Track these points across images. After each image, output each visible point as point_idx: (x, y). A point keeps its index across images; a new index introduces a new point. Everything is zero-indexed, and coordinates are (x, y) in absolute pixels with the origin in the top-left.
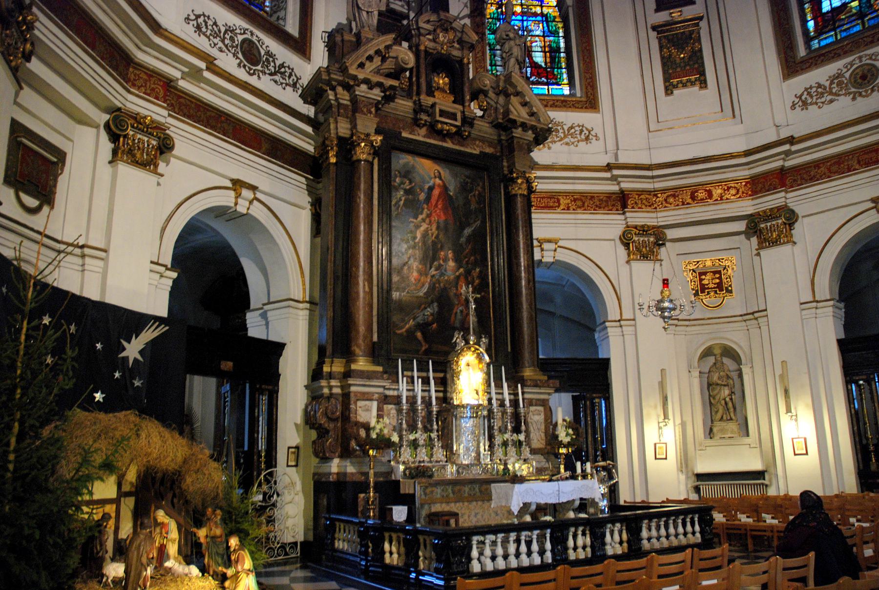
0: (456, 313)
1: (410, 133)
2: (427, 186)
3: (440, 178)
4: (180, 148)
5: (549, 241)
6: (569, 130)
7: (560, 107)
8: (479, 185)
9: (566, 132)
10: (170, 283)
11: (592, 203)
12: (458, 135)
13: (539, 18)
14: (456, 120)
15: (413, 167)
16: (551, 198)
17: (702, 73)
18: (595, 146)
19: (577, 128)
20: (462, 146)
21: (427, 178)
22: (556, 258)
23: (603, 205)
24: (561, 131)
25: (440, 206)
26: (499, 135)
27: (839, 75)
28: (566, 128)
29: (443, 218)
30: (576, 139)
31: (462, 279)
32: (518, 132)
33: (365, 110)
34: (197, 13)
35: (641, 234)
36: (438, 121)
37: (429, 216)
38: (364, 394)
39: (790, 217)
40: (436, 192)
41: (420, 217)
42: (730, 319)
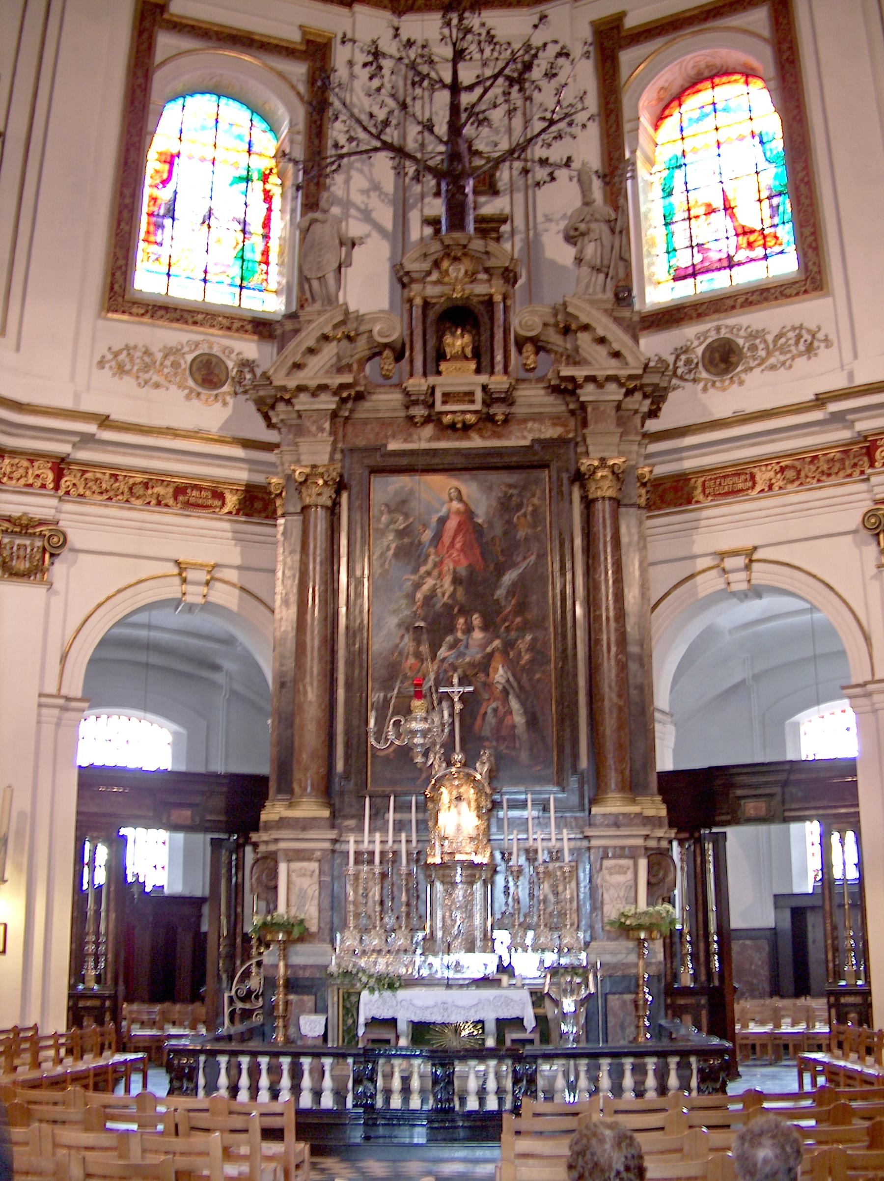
0: (486, 713)
1: (405, 441)
2: (435, 518)
3: (460, 499)
5: (735, 553)
6: (775, 341)
7: (758, 302)
8: (533, 495)
9: (771, 346)
11: (813, 468)
14: (472, 402)
15: (411, 492)
16: (739, 475)
18: (825, 356)
20: (499, 436)
22: (753, 582)
23: (835, 469)
24: (761, 346)
25: (458, 546)
28: (770, 338)
29: (464, 563)
30: (789, 356)
31: (497, 656)
32: (588, 393)
33: (314, 429)
34: (116, 348)
37: (438, 565)
38: (297, 851)
41: (423, 570)
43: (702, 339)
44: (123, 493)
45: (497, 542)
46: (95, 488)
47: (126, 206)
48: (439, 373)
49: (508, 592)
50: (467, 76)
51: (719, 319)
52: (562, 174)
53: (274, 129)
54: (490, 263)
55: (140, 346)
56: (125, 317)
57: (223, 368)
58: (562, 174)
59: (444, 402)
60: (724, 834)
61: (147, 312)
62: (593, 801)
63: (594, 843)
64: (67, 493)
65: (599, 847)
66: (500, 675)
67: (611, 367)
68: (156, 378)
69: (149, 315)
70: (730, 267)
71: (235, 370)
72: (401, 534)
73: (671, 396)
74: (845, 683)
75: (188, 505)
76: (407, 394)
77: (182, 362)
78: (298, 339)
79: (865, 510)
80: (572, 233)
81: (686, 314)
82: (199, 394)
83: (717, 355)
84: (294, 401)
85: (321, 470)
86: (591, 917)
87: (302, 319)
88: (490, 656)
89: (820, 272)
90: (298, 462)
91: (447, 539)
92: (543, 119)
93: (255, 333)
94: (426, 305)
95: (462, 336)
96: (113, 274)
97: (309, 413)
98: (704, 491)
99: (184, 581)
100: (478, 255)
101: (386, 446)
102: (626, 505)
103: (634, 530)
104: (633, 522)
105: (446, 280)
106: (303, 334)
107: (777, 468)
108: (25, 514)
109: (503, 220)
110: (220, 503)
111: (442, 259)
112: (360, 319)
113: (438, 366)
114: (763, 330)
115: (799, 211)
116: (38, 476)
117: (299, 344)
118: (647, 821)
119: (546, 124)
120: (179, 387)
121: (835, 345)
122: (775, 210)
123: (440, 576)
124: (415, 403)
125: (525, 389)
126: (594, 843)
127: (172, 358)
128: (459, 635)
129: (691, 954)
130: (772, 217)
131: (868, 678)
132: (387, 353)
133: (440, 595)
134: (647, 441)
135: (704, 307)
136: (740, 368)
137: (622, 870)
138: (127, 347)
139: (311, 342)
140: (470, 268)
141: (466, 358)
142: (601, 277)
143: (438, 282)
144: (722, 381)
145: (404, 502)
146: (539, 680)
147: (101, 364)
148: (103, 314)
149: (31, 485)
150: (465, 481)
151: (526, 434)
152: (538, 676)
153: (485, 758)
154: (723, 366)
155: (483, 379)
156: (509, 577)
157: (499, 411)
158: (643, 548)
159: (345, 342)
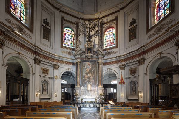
4: (146, 58)
10: (7, 68)
12: (92, 58)
17: (136, 36)
18: (117, 53)
27: (155, 30)
39: (58, 67)
42: (135, 77)
50: (90, 27)
66: (92, 77)
67: (100, 54)
156: (93, 70)
157: (92, 57)
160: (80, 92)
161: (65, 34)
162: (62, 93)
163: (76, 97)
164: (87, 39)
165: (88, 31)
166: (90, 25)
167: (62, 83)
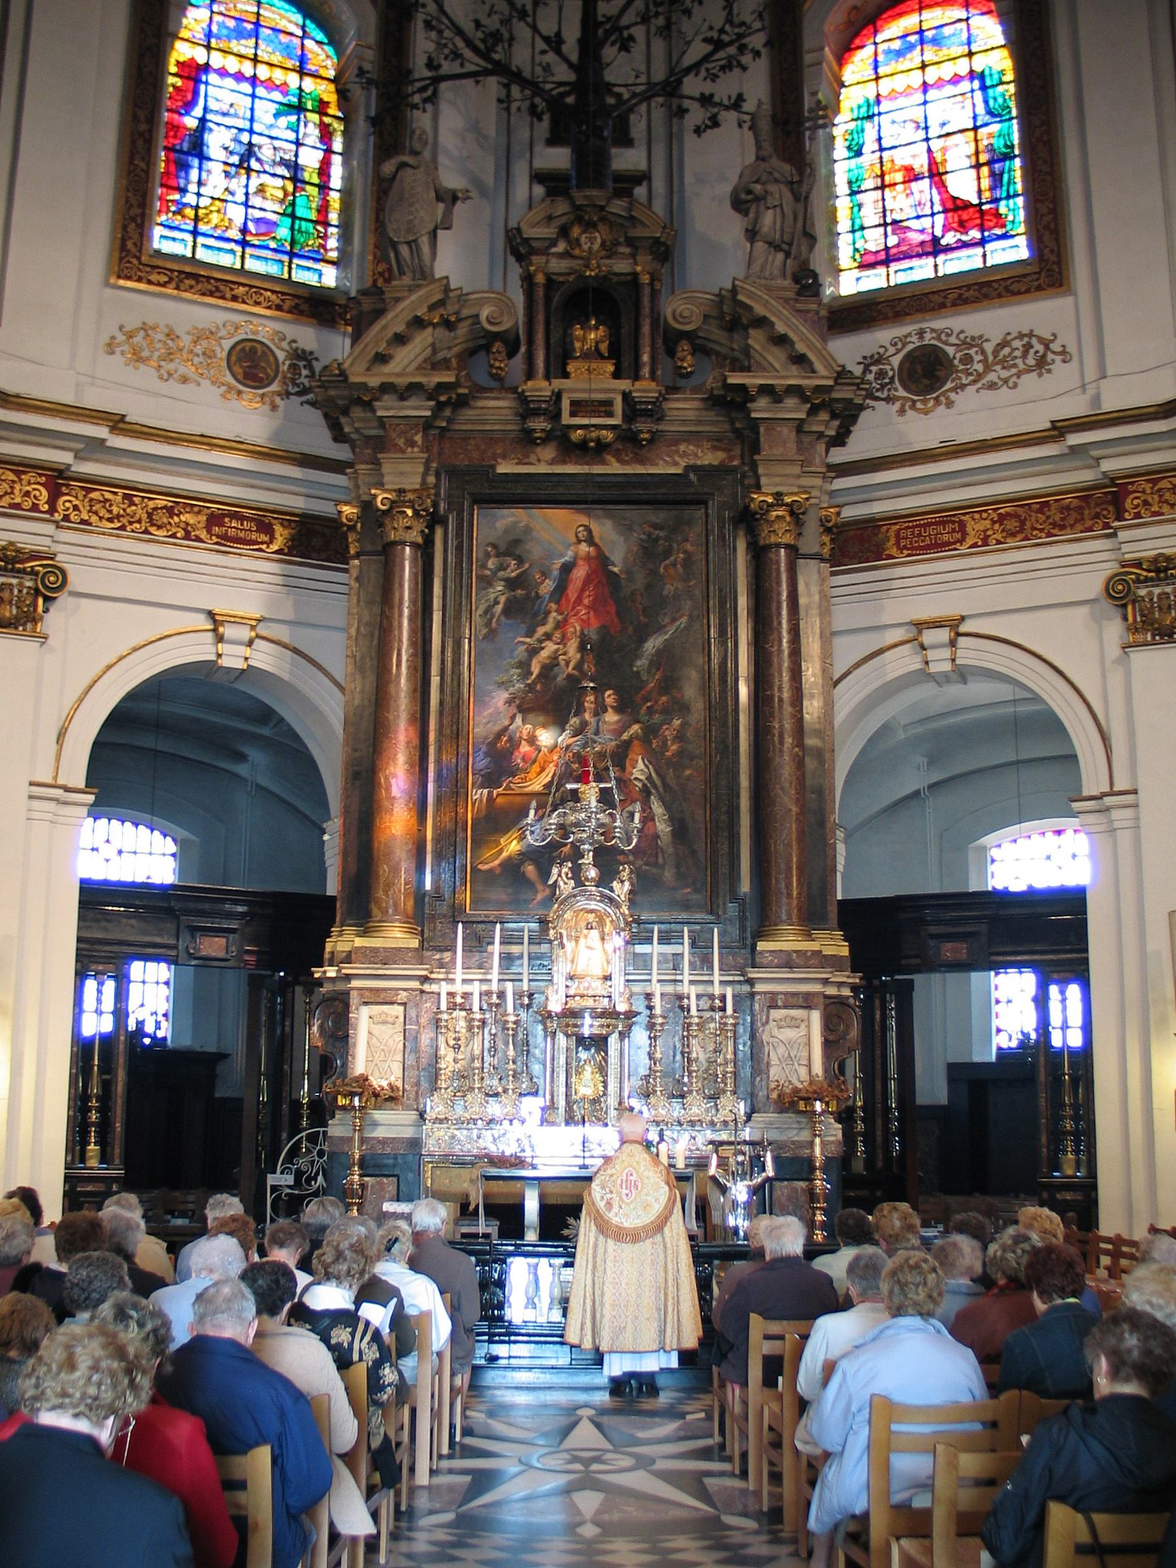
3: (590, 540)
5: (936, 624)
6: (996, 352)
7: (976, 300)
9: (991, 358)
11: (1042, 517)
13: (965, 86)
14: (610, 414)
15: (528, 530)
16: (943, 523)
18: (1062, 374)
19: (1017, 344)
20: (642, 462)
21: (560, 547)
25: (586, 601)
26: (732, 422)
28: (989, 347)
29: (595, 624)
30: (1014, 371)
31: (636, 746)
33: (401, 442)
35: (1152, 579)
36: (570, 427)
40: (580, 573)
41: (541, 630)
43: (899, 346)
44: (139, 521)
45: (639, 598)
46: (102, 513)
47: (141, 134)
48: (566, 375)
49: (651, 662)
51: (924, 320)
52: (729, 118)
53: (334, 40)
54: (639, 232)
55: (162, 325)
56: (142, 286)
57: (271, 359)
58: (729, 118)
59: (573, 414)
60: (912, 980)
61: (171, 280)
62: (761, 933)
63: (759, 988)
64: (66, 518)
65: (765, 993)
68: (182, 370)
69: (173, 285)
70: (935, 254)
71: (287, 363)
72: (511, 584)
73: (864, 416)
74: (1074, 795)
75: (225, 538)
76: (523, 399)
77: (218, 350)
78: (382, 322)
79: (1108, 573)
80: (743, 196)
81: (879, 312)
82: (239, 393)
83: (919, 368)
84: (377, 404)
85: (410, 496)
86: (753, 1083)
87: (387, 295)
88: (626, 745)
89: (1059, 263)
90: (380, 485)
91: (572, 593)
92: (707, 40)
93: (312, 316)
94: (550, 283)
95: (596, 328)
96: (125, 227)
97: (396, 421)
98: (897, 544)
99: (220, 639)
100: (619, 220)
101: (493, 467)
102: (806, 557)
103: (815, 589)
104: (815, 577)
105: (577, 252)
106: (390, 315)
107: (995, 516)
108: (11, 543)
109: (642, 178)
110: (266, 539)
111: (572, 223)
112: (463, 298)
113: (564, 365)
114: (981, 337)
115: (1034, 180)
116: (27, 494)
117: (384, 328)
118: (822, 960)
119: (710, 48)
120: (214, 383)
121: (1075, 358)
122: (996, 178)
123: (563, 640)
124: (536, 413)
125: (678, 400)
126: (759, 988)
127: (204, 343)
128: (587, 716)
129: (863, 1135)
130: (992, 189)
131: (1106, 788)
132: (497, 346)
133: (563, 663)
134: (833, 474)
135: (904, 303)
136: (949, 385)
137: (794, 1024)
138: (144, 328)
139: (400, 328)
140: (608, 238)
141: (602, 357)
142: (780, 256)
143: (566, 255)
144: (924, 402)
145: (517, 542)
146: (688, 778)
147: (110, 348)
148: (113, 280)
149: (17, 506)
150: (597, 517)
151: (677, 459)
152: (688, 772)
153: (625, 875)
154: (926, 382)
155: (624, 385)
157: (643, 427)
158: (825, 611)
159: (441, 332)
160: (410, 1040)
161: (194, 72)
162: (83, 1050)
163: (337, 1128)
164: (552, 142)
165: (572, 34)
166: (99, 1384)
167: (97, 872)
